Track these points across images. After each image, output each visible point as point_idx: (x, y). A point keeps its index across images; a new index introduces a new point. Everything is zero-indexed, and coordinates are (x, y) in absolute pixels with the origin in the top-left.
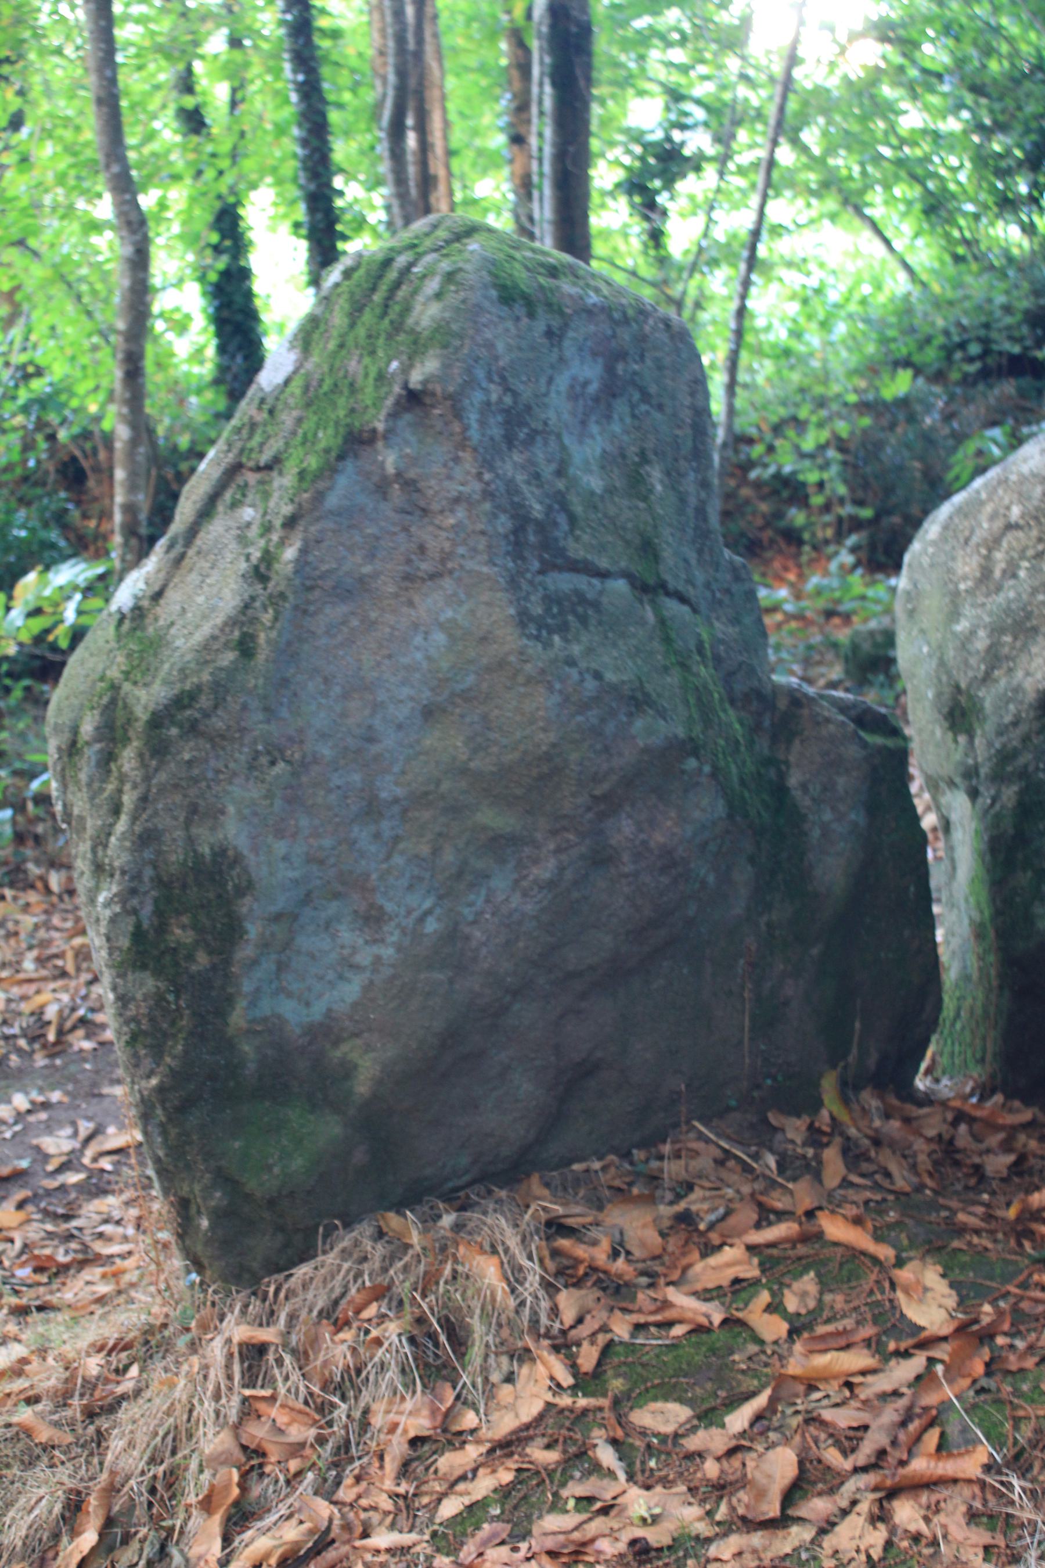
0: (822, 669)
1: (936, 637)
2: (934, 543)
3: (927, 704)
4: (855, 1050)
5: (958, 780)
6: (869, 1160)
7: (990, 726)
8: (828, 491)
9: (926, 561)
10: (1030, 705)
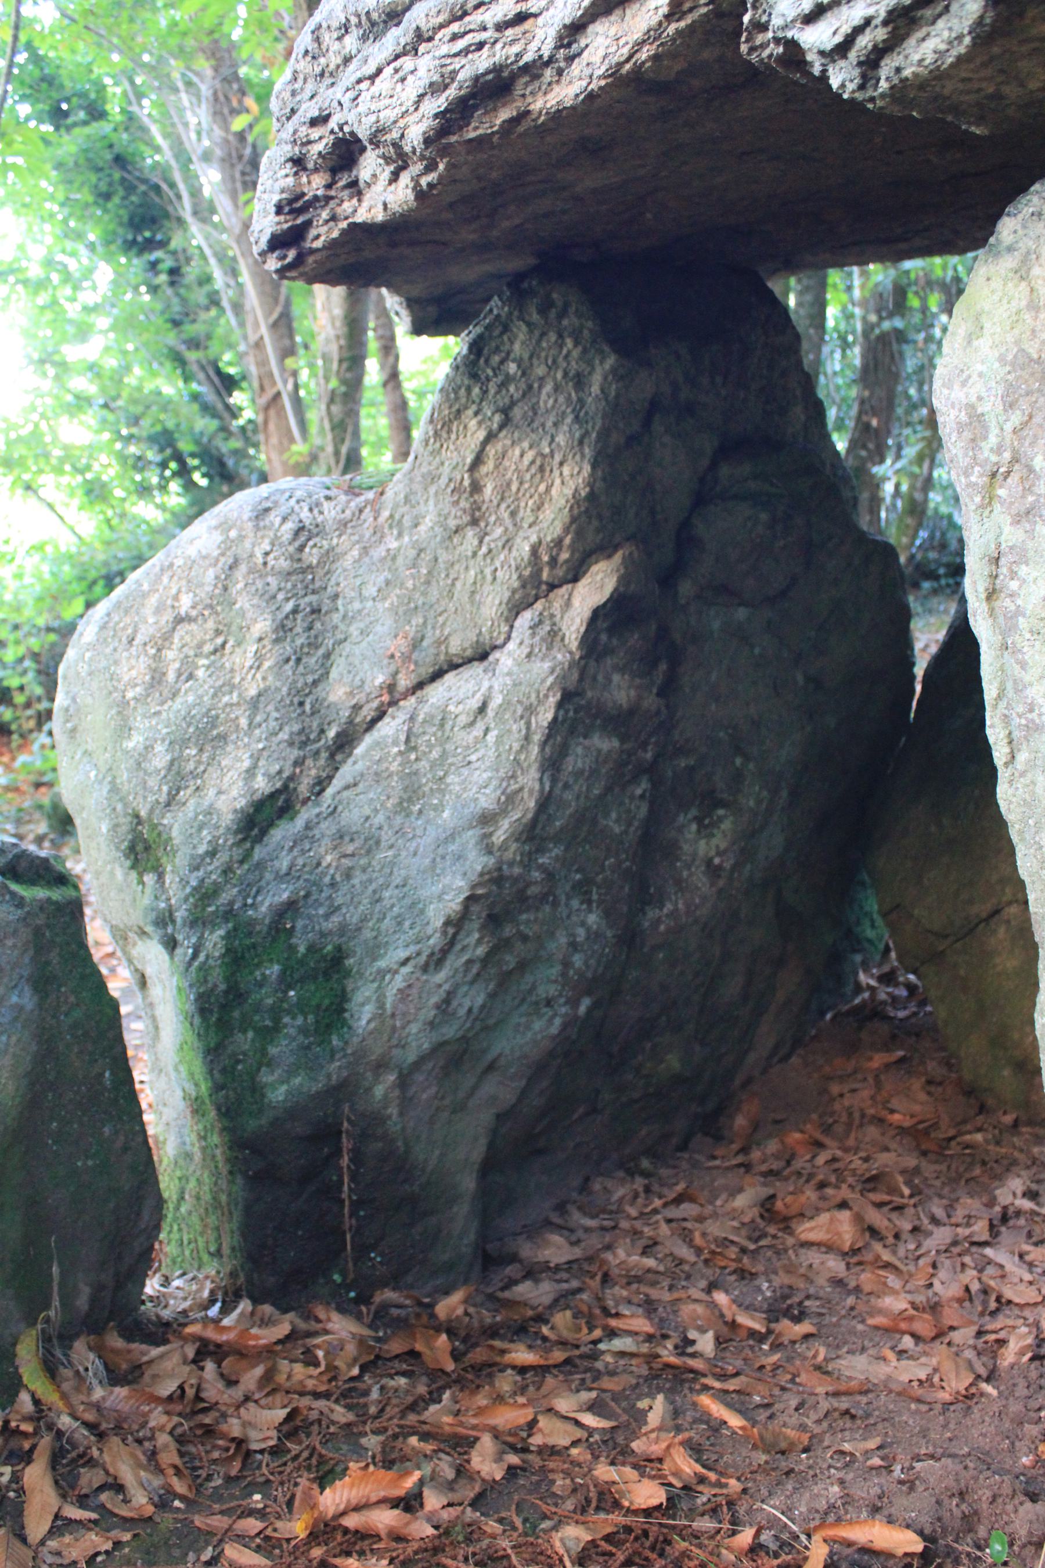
0: (31, 827)
1: (104, 759)
2: (91, 647)
3: (101, 839)
4: (56, 1302)
5: (149, 929)
6: (91, 1463)
7: (182, 860)
8: (27, 692)
9: (84, 669)
10: (228, 829)
